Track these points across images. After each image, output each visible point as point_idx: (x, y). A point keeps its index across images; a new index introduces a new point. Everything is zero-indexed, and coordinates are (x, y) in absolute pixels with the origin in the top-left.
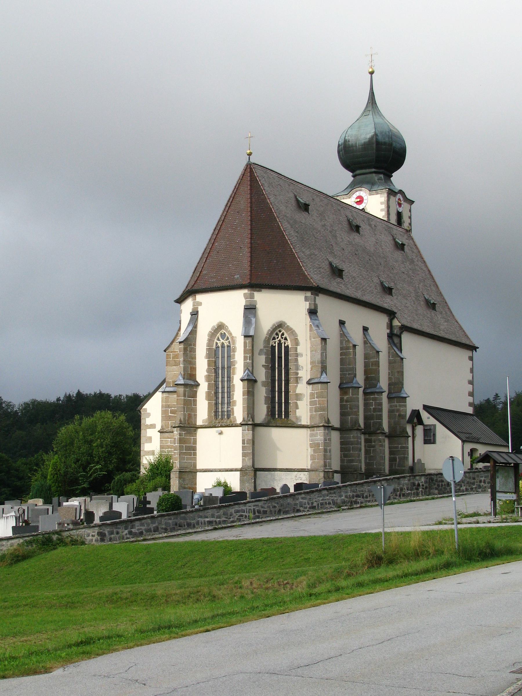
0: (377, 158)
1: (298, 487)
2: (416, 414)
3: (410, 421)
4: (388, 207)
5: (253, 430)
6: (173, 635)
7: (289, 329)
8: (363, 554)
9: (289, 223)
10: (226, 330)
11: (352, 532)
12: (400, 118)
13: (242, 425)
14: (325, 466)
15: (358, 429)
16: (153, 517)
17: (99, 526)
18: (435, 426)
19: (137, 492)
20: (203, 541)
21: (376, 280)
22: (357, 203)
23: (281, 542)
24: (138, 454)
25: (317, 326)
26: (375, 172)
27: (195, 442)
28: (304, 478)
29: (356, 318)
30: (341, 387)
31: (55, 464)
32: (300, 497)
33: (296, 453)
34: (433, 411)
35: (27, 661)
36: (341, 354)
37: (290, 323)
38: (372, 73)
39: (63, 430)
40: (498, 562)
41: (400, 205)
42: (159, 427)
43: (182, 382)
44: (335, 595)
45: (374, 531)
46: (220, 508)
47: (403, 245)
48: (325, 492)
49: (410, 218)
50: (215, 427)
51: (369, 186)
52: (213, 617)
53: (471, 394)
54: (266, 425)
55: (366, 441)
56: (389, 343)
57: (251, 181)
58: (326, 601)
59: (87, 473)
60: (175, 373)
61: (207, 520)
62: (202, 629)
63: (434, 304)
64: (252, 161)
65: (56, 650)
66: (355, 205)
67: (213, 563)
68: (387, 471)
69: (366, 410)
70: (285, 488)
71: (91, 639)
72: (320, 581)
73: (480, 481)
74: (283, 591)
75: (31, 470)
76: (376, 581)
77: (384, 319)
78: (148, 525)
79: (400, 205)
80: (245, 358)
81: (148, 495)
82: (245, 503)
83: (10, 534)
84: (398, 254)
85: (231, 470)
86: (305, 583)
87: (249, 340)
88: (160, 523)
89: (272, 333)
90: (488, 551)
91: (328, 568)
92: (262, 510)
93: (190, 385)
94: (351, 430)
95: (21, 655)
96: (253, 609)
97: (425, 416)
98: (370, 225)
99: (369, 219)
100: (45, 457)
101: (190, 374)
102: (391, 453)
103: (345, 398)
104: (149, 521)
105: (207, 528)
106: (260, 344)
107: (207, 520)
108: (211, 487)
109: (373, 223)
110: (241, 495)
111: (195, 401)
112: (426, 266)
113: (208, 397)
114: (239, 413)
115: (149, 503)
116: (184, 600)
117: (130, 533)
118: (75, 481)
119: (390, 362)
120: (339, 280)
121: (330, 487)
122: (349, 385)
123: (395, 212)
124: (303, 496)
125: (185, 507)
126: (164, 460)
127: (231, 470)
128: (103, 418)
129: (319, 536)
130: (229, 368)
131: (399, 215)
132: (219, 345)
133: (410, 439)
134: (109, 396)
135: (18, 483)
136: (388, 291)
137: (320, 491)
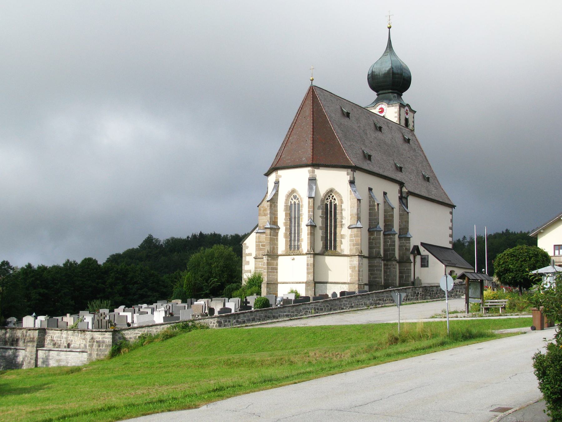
0: (392, 83)
1: (342, 293)
2: (416, 248)
3: (412, 253)
4: (400, 115)
5: (314, 258)
6: (274, 386)
7: (337, 193)
8: (387, 335)
9: (337, 125)
10: (297, 193)
11: (378, 323)
12: (407, 57)
13: (307, 254)
14: (359, 280)
15: (380, 258)
16: (251, 312)
17: (218, 317)
18: (428, 256)
19: (240, 296)
20: (284, 327)
21: (392, 162)
22: (380, 112)
23: (333, 328)
24: (240, 272)
25: (355, 191)
26: (391, 92)
27: (277, 265)
28: (345, 288)
29: (380, 187)
30: (369, 231)
31: (188, 278)
32: (344, 300)
33: (342, 272)
34: (426, 246)
35: (183, 401)
36: (370, 210)
37: (337, 189)
38: (389, 28)
39: (193, 256)
40: (474, 342)
41: (407, 114)
42: (254, 255)
43: (269, 226)
44: (373, 362)
45: (392, 322)
46: (293, 306)
47: (409, 140)
48: (359, 297)
49: (413, 122)
50: (289, 255)
51: (388, 101)
52: (298, 374)
53: (451, 236)
54: (322, 254)
55: (385, 265)
56: (400, 203)
57: (313, 97)
58: (368, 365)
59: (208, 283)
60: (264, 221)
61: (285, 314)
62: (292, 382)
63: (428, 178)
64: (314, 84)
65: (201, 394)
66: (379, 114)
67: (290, 341)
68: (398, 284)
69: (385, 245)
70: (334, 294)
71: (223, 387)
72: (358, 352)
73: (457, 291)
74: (335, 359)
75: (172, 281)
76: (399, 353)
77: (396, 187)
78: (248, 316)
79: (407, 114)
80: (309, 212)
81: (247, 298)
82: (309, 304)
83: (162, 321)
84: (406, 146)
85: (300, 283)
86: (349, 354)
87: (311, 200)
88: (256, 316)
89: (326, 195)
90: (468, 335)
91: (364, 345)
92: (320, 308)
93: (274, 229)
94: (375, 258)
95: (179, 396)
96: (322, 369)
97: (422, 249)
98: (388, 126)
99: (387, 123)
100: (181, 273)
101: (274, 221)
102: (400, 273)
103: (372, 237)
104: (249, 314)
105: (285, 319)
106: (318, 203)
107: (285, 314)
108: (287, 293)
109: (390, 125)
110: (307, 299)
111: (277, 239)
112: (424, 154)
113: (286, 236)
114: (305, 246)
115: (249, 303)
116: (273, 364)
117: (237, 321)
118: (201, 289)
119: (400, 215)
120: (369, 162)
121: (362, 295)
122: (375, 229)
123: (404, 118)
124: (346, 299)
125: (271, 305)
126: (257, 275)
127: (283, 283)
128: (217, 249)
129: (357, 325)
130: (299, 218)
131: (407, 120)
132: (293, 203)
133: (412, 264)
134: (220, 235)
135: (164, 290)
136: (400, 169)
137: (356, 296)
